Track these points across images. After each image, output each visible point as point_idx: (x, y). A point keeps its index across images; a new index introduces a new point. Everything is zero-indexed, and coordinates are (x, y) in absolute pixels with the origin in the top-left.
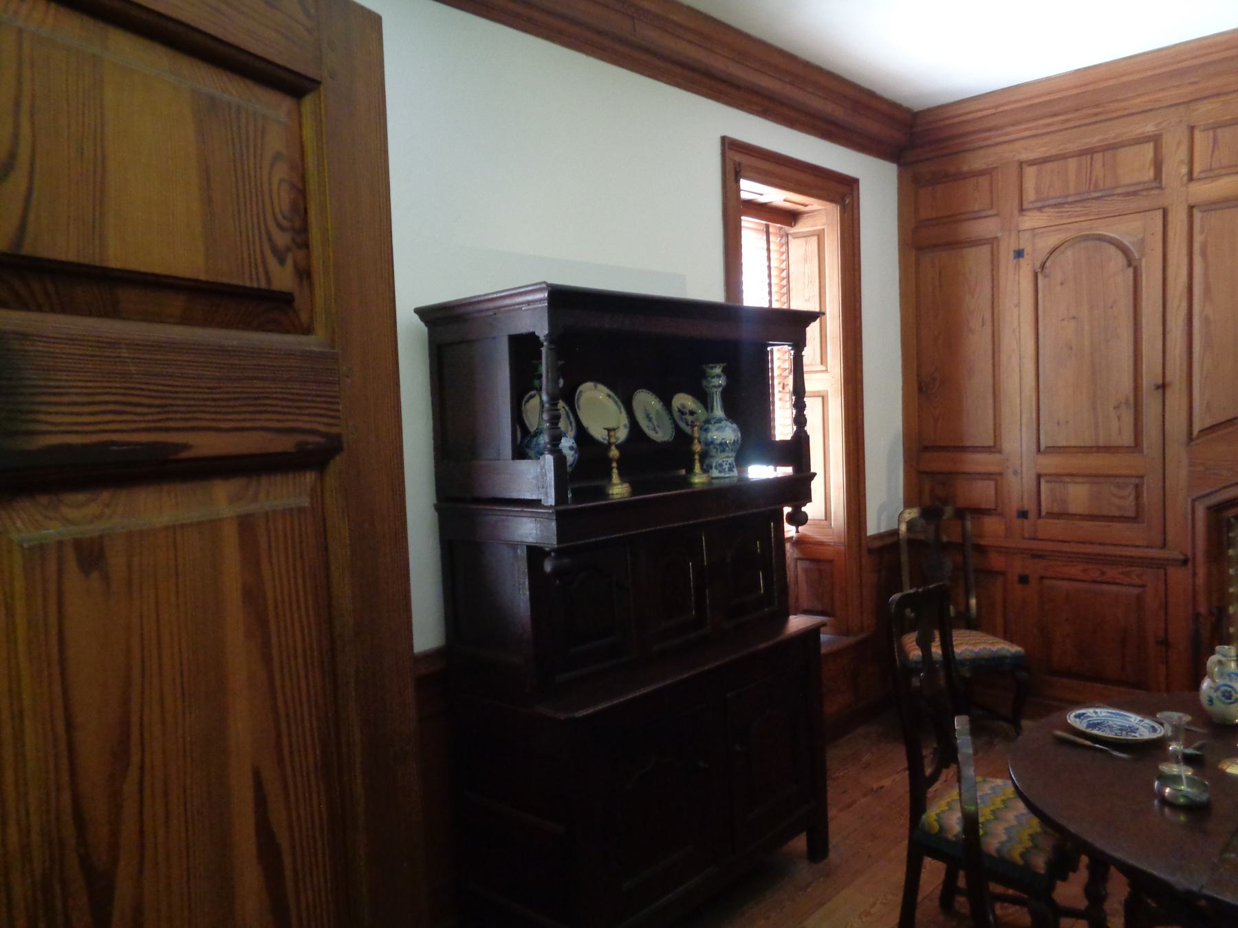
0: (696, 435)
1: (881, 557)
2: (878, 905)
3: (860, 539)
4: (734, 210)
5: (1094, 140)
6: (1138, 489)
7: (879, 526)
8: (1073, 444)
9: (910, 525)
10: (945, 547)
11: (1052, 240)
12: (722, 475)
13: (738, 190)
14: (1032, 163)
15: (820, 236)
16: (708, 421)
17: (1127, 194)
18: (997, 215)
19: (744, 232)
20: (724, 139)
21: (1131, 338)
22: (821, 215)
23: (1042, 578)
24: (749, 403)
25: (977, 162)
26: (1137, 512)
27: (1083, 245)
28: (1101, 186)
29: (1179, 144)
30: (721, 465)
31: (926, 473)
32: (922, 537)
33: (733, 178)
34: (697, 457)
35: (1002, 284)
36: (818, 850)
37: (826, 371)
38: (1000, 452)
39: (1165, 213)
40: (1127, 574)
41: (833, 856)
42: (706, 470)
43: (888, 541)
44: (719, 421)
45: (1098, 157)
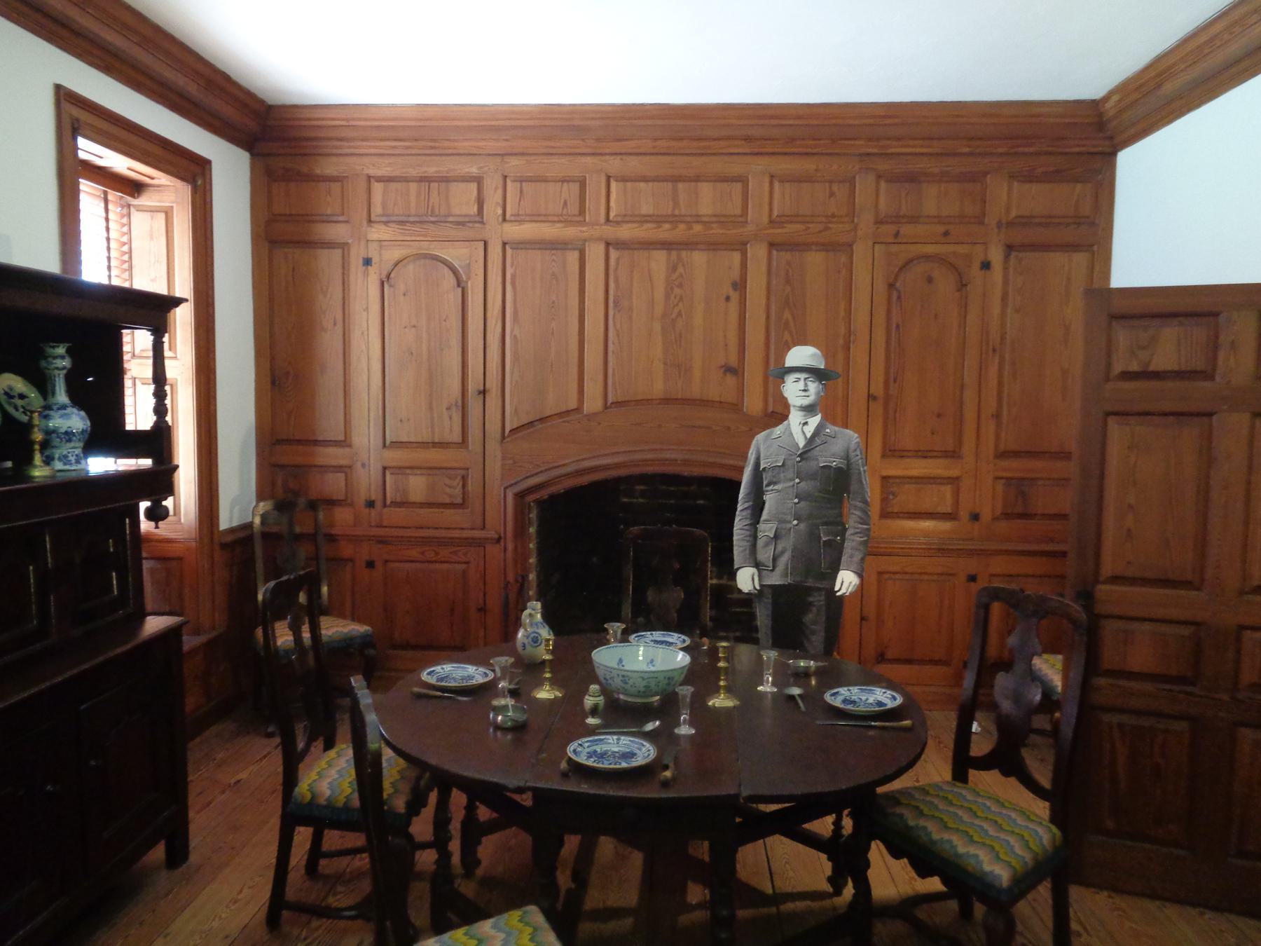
0: (36, 422)
1: (235, 551)
2: (245, 890)
3: (212, 533)
4: (71, 169)
5: (431, 171)
6: (464, 478)
7: (231, 521)
8: (412, 440)
9: (264, 517)
10: (298, 538)
11: (397, 254)
12: (67, 467)
13: (76, 148)
14: (379, 179)
15: (168, 214)
16: (48, 407)
17: (458, 223)
18: (347, 222)
19: (82, 197)
20: (58, 88)
21: (460, 350)
22: (169, 191)
23: (386, 561)
24: (100, 390)
25: (329, 167)
26: (463, 499)
27: (423, 261)
28: (437, 212)
29: (496, 189)
30: (66, 457)
31: (278, 466)
32: (275, 529)
33: (70, 133)
34: (37, 447)
35: (352, 288)
36: (177, 855)
37: (175, 358)
38: (350, 446)
39: (486, 244)
40: (455, 553)
41: (194, 858)
42: (48, 461)
43: (241, 535)
44: (64, 407)
45: (434, 185)
